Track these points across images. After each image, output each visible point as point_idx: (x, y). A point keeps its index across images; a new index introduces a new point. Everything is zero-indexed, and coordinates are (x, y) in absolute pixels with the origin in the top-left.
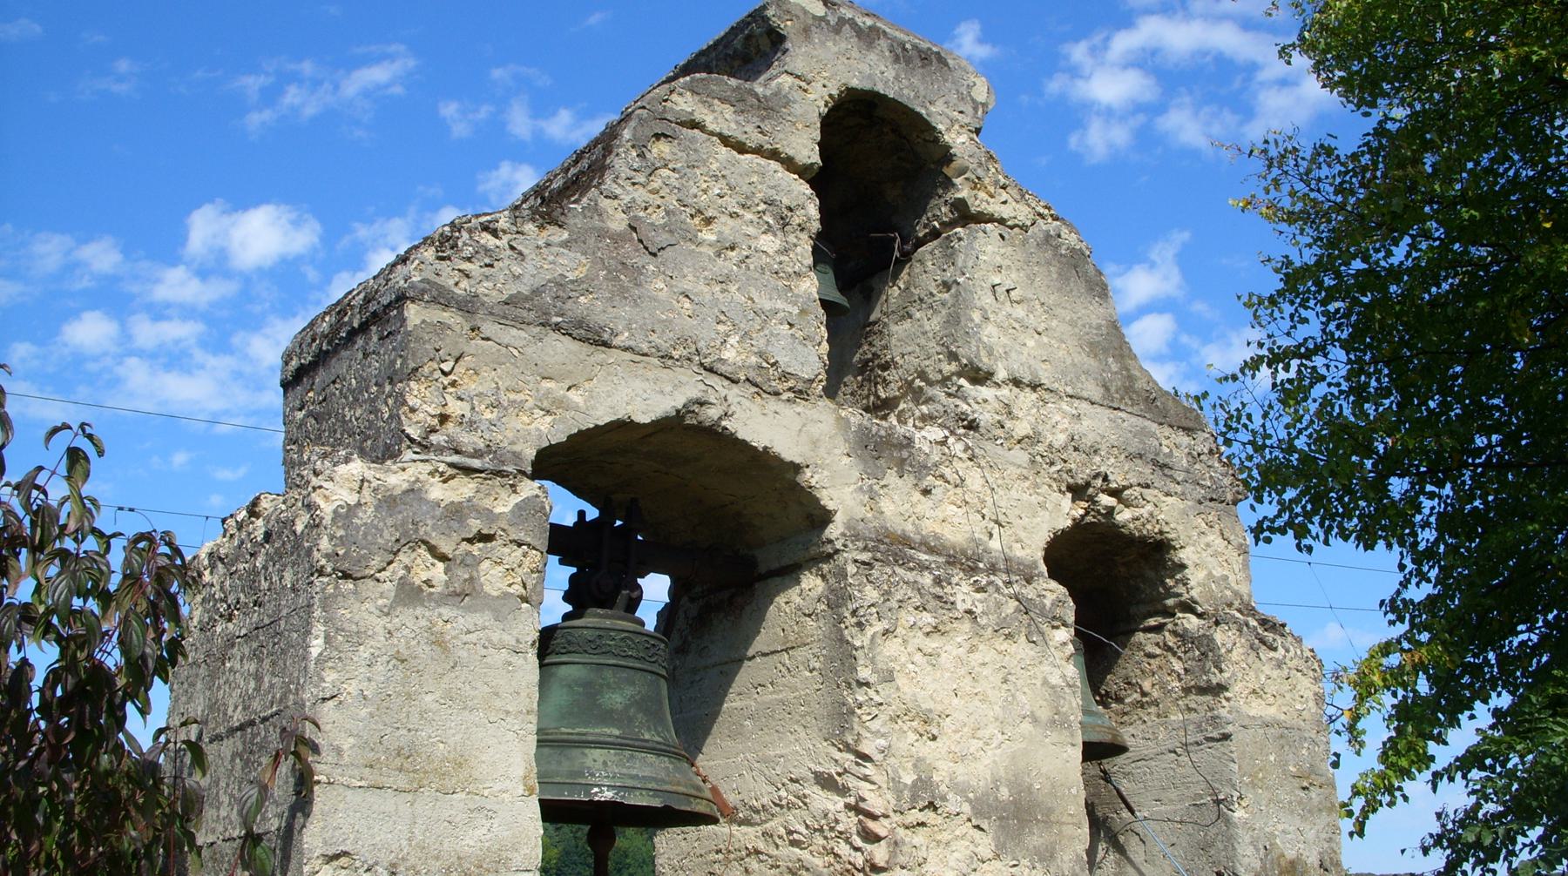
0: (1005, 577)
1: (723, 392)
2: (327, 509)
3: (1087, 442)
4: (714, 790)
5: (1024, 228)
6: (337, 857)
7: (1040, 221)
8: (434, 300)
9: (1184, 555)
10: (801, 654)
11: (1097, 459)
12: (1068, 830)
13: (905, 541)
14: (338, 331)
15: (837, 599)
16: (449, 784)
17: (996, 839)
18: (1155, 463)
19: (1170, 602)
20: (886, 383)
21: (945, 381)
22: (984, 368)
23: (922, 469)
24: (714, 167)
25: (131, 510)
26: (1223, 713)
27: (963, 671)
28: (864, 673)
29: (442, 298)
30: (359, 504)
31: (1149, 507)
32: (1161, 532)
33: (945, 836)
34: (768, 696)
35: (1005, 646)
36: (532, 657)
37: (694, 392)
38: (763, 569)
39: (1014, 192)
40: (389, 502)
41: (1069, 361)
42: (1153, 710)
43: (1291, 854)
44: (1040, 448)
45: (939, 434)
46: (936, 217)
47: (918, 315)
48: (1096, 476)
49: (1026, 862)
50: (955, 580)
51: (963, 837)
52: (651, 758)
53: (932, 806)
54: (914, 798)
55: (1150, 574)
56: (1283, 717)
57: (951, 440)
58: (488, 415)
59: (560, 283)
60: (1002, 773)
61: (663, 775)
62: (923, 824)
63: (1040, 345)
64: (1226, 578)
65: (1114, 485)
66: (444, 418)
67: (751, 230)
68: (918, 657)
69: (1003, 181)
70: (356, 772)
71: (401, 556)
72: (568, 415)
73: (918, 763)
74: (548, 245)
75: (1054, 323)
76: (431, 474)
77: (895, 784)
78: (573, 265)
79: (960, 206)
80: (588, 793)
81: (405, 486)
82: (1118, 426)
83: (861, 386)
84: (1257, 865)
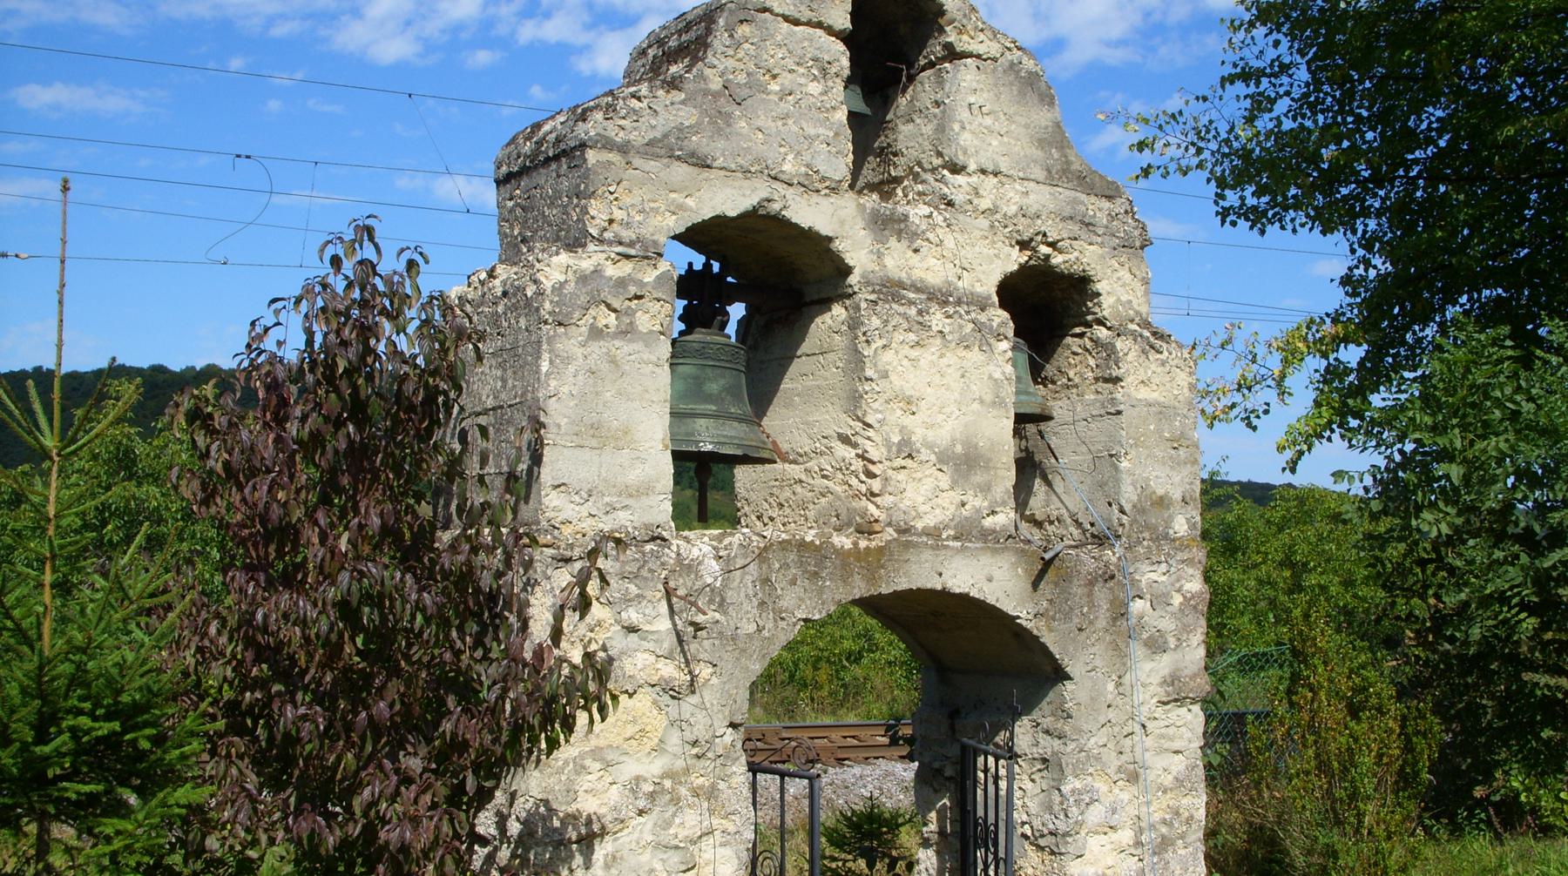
0: (966, 308)
1: (783, 192)
2: (547, 285)
3: (1033, 210)
4: (774, 443)
5: (995, 60)
6: (559, 486)
7: (1008, 53)
8: (604, 147)
9: (1099, 287)
10: (830, 356)
11: (1039, 222)
12: (1001, 473)
13: (901, 285)
14: (537, 155)
15: (854, 324)
16: (620, 444)
17: (952, 477)
18: (1082, 222)
19: (1089, 318)
20: (896, 166)
21: (934, 170)
22: (961, 164)
23: (914, 235)
24: (779, 38)
25: (248, 157)
26: (1119, 396)
27: (934, 370)
28: (869, 373)
29: (608, 144)
30: (566, 281)
31: (1076, 254)
32: (1084, 271)
33: (919, 475)
34: (809, 382)
35: (964, 353)
36: (667, 368)
37: (765, 194)
38: (808, 299)
39: (989, 34)
40: (583, 279)
41: (1022, 154)
42: (1074, 390)
43: (1160, 492)
44: (998, 216)
45: (926, 210)
46: (933, 53)
47: (918, 121)
48: (1037, 234)
49: (972, 492)
50: (932, 311)
51: (931, 475)
52: (736, 424)
53: (910, 456)
54: (899, 451)
55: (1076, 297)
56: (1162, 399)
57: (935, 214)
58: (638, 218)
59: (680, 128)
60: (958, 436)
61: (742, 435)
62: (904, 468)
63: (1001, 143)
64: (1130, 302)
65: (1050, 240)
66: (611, 221)
67: (803, 81)
68: (905, 362)
69: (981, 25)
70: (569, 438)
71: (591, 311)
72: (686, 214)
73: (902, 429)
74: (672, 104)
75: (1013, 127)
76: (606, 259)
77: (888, 443)
78: (688, 116)
79: (949, 47)
80: (697, 446)
81: (592, 268)
82: (1055, 198)
83: (879, 165)
84: (1135, 498)
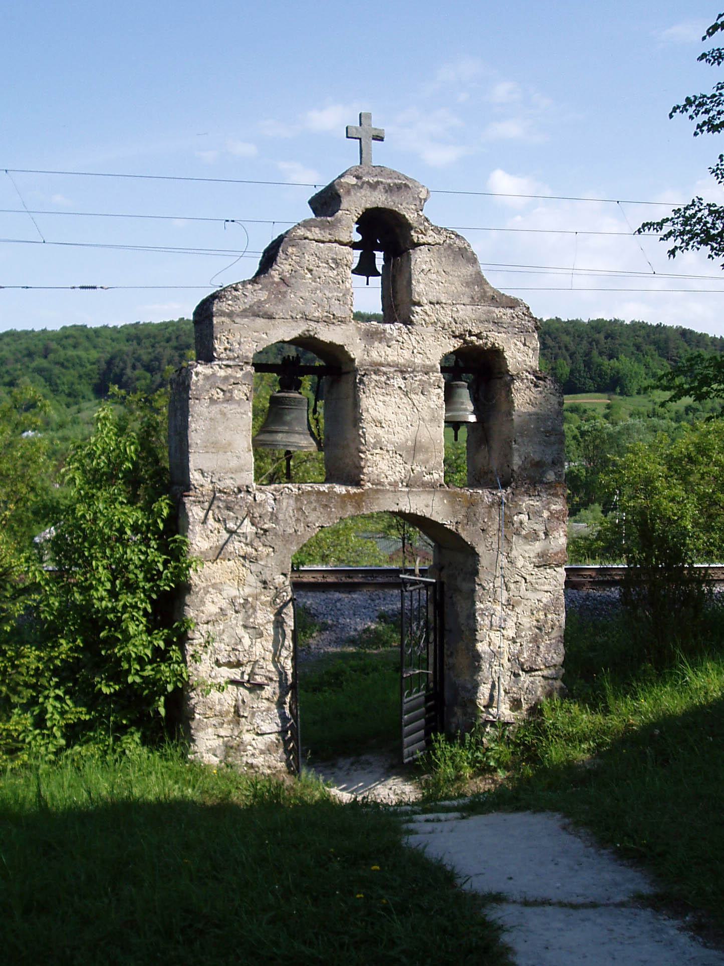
1: (315, 326)
25: (233, 221)
55: (497, 359)
59: (260, 301)
